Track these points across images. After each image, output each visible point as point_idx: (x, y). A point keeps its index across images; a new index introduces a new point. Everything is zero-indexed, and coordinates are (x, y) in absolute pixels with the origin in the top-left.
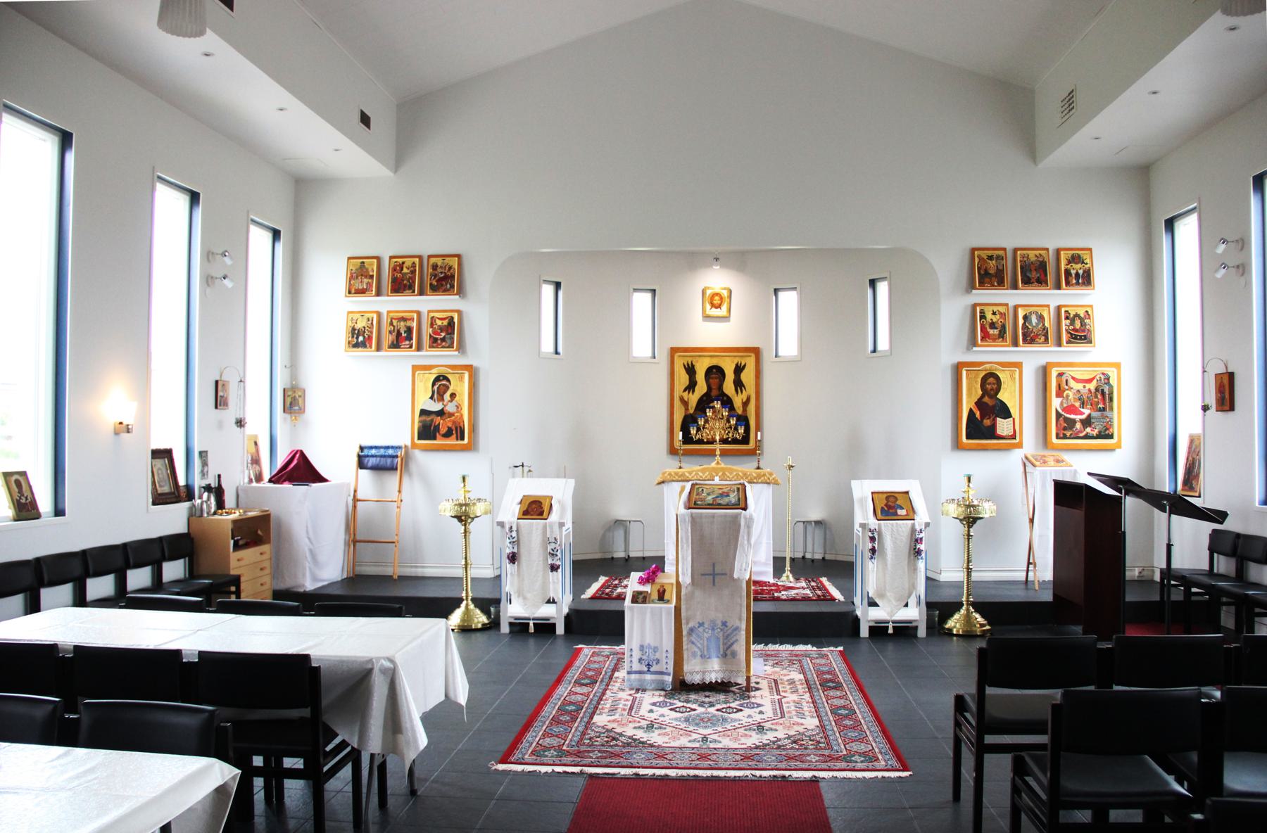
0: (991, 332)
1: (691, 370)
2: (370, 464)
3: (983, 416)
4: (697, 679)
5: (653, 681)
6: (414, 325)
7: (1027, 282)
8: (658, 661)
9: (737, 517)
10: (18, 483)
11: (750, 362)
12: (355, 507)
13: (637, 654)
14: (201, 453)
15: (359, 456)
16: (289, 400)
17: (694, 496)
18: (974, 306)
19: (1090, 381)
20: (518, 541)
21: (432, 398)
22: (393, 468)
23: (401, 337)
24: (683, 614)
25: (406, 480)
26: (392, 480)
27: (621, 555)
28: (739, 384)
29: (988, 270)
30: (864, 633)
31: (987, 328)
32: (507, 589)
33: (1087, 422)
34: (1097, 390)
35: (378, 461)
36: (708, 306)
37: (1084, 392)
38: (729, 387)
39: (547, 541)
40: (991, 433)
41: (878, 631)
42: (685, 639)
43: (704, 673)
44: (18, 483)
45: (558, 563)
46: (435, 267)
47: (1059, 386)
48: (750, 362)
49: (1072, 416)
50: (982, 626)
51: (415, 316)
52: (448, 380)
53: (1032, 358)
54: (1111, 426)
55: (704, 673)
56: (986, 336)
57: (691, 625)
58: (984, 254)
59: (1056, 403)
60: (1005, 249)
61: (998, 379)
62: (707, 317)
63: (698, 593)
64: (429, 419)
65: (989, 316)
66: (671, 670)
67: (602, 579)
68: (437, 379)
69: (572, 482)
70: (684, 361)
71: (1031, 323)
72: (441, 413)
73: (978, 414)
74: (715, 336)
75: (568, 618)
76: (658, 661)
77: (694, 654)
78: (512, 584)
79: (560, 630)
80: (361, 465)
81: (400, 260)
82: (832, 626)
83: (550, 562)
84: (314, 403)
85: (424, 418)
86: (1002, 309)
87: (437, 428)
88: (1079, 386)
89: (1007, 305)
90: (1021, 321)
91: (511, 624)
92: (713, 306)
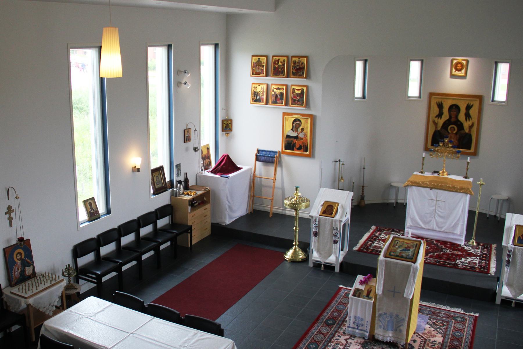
1: (440, 106)
2: (262, 160)
4: (380, 338)
5: (359, 333)
6: (284, 92)
8: (363, 325)
9: (410, 266)
10: (90, 204)
12: (254, 180)
13: (352, 320)
14: (177, 166)
15: (256, 155)
16: (225, 125)
17: (392, 248)
20: (319, 226)
21: (292, 129)
22: (273, 162)
23: (278, 99)
24: (377, 307)
25: (279, 169)
26: (272, 168)
28: (468, 116)
30: (498, 301)
32: (312, 248)
35: (265, 157)
36: (454, 70)
38: (462, 117)
39: (332, 229)
41: (506, 302)
42: (376, 318)
43: (384, 336)
44: (90, 204)
46: (295, 63)
48: (476, 104)
51: (285, 87)
52: (300, 121)
55: (384, 336)
57: (381, 312)
62: (452, 76)
64: (291, 140)
66: (368, 330)
67: (373, 227)
68: (295, 121)
69: (352, 194)
70: (436, 101)
72: (296, 138)
75: (342, 264)
77: (380, 326)
78: (314, 246)
79: (337, 270)
80: (258, 159)
81: (277, 58)
84: (236, 126)
85: (288, 139)
87: (294, 145)
91: (314, 263)
92: (457, 70)
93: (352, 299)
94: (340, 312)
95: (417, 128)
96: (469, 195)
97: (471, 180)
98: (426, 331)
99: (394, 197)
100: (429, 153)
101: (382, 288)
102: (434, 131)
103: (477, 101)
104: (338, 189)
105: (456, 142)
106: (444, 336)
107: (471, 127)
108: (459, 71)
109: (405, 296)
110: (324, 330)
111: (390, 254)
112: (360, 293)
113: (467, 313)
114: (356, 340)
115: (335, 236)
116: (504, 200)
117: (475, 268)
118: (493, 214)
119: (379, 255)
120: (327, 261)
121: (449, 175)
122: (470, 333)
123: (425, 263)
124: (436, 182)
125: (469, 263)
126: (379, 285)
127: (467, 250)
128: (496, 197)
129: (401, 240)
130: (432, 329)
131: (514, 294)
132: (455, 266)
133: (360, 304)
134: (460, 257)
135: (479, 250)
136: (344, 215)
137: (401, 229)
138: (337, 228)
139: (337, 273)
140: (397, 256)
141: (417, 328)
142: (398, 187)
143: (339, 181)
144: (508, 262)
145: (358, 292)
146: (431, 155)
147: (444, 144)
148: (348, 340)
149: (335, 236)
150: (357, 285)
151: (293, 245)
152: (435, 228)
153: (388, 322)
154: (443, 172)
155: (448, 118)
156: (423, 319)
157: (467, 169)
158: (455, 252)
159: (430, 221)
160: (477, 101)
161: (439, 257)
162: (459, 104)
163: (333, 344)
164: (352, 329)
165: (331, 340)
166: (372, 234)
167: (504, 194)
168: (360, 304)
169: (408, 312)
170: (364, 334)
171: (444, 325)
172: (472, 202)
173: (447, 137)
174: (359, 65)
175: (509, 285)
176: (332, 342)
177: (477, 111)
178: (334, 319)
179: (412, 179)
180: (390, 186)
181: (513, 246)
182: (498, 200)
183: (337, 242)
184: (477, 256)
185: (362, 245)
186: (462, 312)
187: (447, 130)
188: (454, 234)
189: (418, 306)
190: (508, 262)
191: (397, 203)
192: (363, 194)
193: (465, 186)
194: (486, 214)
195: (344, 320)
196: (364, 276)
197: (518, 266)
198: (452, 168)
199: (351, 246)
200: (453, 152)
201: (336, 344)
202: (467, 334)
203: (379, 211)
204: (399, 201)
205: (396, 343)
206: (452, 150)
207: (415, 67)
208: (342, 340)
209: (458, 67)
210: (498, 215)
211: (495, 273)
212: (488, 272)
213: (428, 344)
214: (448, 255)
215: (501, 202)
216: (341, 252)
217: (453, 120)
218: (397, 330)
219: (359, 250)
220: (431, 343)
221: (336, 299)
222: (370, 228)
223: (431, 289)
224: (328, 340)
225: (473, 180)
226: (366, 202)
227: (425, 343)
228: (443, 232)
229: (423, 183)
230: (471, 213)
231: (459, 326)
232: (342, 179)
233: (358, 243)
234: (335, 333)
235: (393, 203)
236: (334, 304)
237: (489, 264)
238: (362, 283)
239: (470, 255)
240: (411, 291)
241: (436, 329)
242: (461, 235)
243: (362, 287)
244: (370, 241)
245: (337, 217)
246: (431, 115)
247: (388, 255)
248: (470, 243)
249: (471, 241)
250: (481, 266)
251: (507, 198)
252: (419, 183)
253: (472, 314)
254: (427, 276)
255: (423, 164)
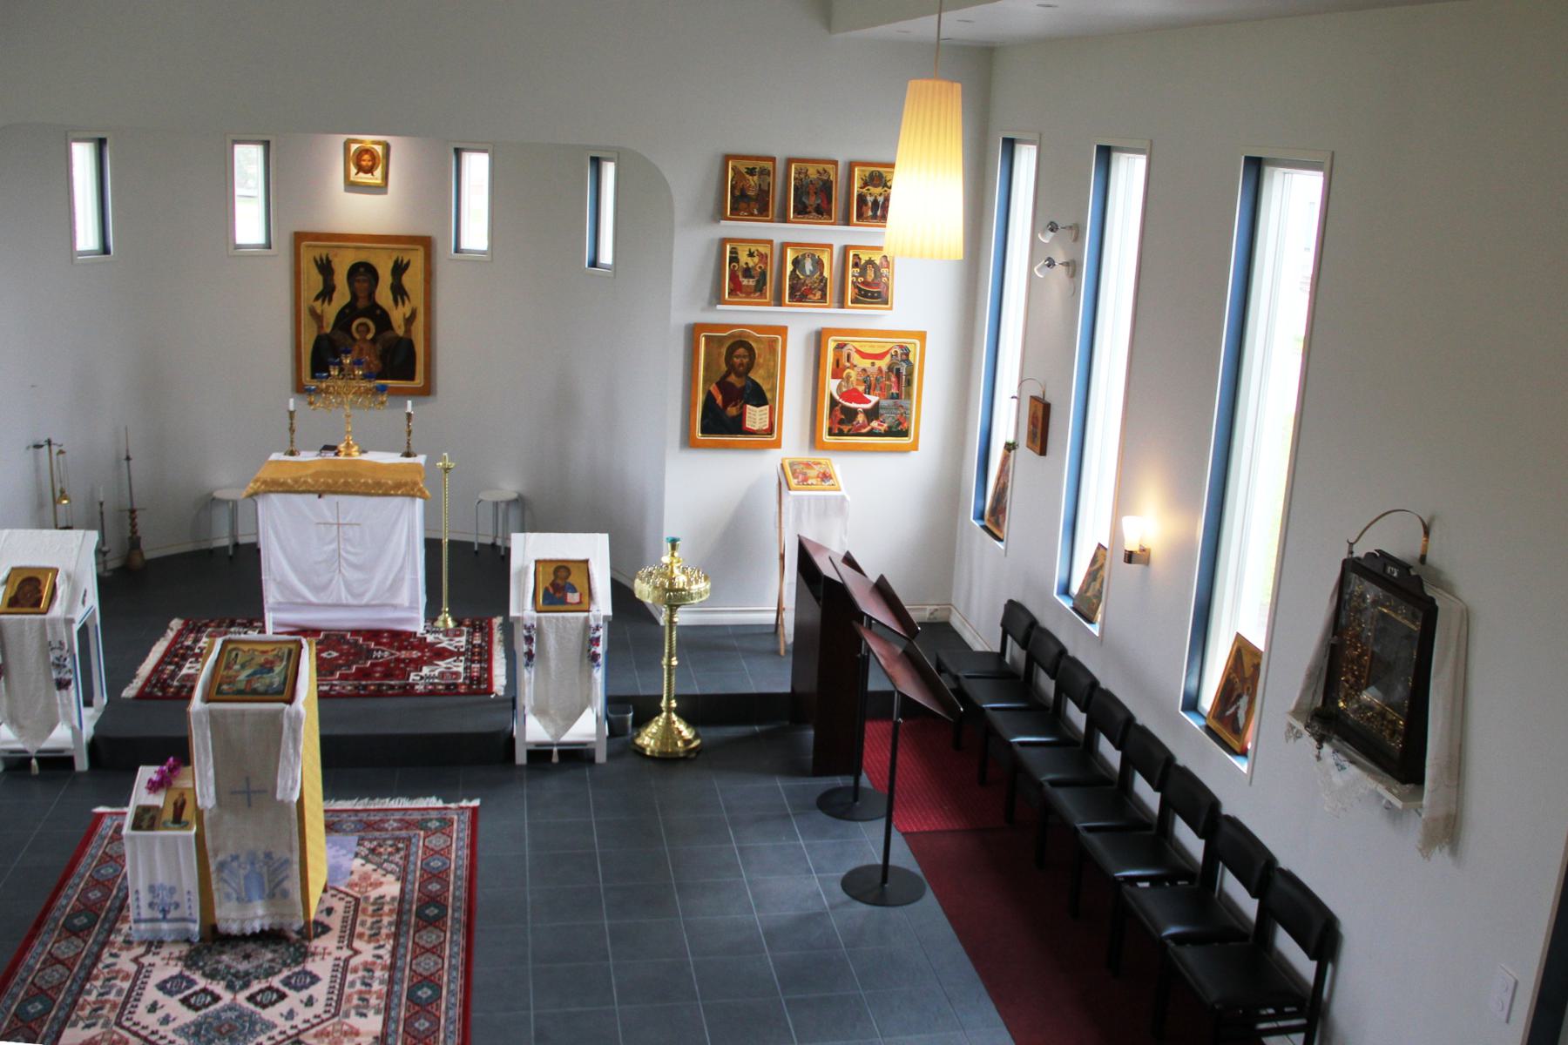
0: (745, 282)
1: (325, 268)
3: (726, 403)
4: (234, 928)
5: (171, 931)
7: (802, 211)
8: (177, 906)
9: (276, 717)
11: (417, 259)
13: (145, 898)
17: (222, 672)
18: (724, 241)
19: (880, 356)
24: (209, 844)
27: (225, 542)
28: (399, 292)
29: (747, 191)
30: (521, 758)
31: (742, 277)
33: (873, 414)
34: (890, 369)
36: (353, 170)
37: (873, 371)
38: (384, 296)
39: (47, 647)
40: (736, 426)
41: (539, 755)
42: (213, 877)
45: (69, 676)
47: (837, 362)
48: (417, 259)
49: (853, 405)
50: (687, 742)
53: (798, 323)
54: (907, 419)
55: (243, 921)
56: (736, 288)
57: (221, 857)
58: (743, 166)
59: (832, 386)
60: (773, 159)
61: (750, 349)
62: (351, 186)
63: (227, 817)
65: (743, 257)
66: (197, 916)
67: (176, 624)
69: (94, 536)
70: (313, 251)
71: (803, 271)
73: (719, 399)
74: (363, 213)
75: (93, 746)
76: (177, 906)
77: (228, 896)
79: (82, 764)
82: (470, 752)
83: (55, 675)
86: (763, 249)
88: (866, 363)
89: (770, 242)
90: (789, 268)
92: (360, 169)
93: (132, 838)
94: (105, 885)
95: (269, 329)
96: (419, 502)
97: (421, 459)
98: (355, 878)
99: (226, 531)
100: (306, 398)
101: (212, 789)
102: (315, 335)
103: (419, 250)
104: (56, 527)
105: (376, 364)
106: (403, 878)
107: (409, 321)
108: (366, 172)
109: (279, 796)
110: (65, 950)
111: (219, 692)
112: (153, 819)
113: (452, 805)
114: (165, 952)
115: (59, 666)
116: (509, 503)
117: (456, 686)
118: (489, 541)
119: (189, 697)
120: (46, 745)
121: (364, 452)
122: (466, 852)
123: (322, 696)
124: (331, 474)
125: (442, 675)
126: (202, 782)
127: (432, 645)
128: (489, 496)
129: (246, 648)
130: (370, 867)
131: (552, 731)
132: (408, 690)
133: (157, 847)
134: (418, 664)
135: (464, 639)
136: (77, 600)
137: (254, 617)
138: (61, 643)
139: (81, 774)
140: (240, 692)
141: (330, 875)
142: (235, 503)
143: (56, 502)
144: (530, 655)
145: (147, 817)
146: (311, 403)
147: (341, 370)
148: (350, 953)
149: (59, 666)
150: (141, 796)
151: (659, 712)
152: (345, 598)
153: (246, 877)
154: (348, 446)
155: (347, 299)
156: (342, 847)
157: (409, 433)
158: (403, 654)
159: (331, 581)
160: (419, 250)
161: (364, 674)
162: (373, 260)
163: (98, 983)
164: (149, 926)
165: (90, 973)
166: (174, 641)
167: (509, 488)
168: (157, 847)
169: (296, 838)
170: (187, 930)
171: (398, 850)
172: (430, 516)
173: (347, 352)
174: (82, 156)
175: (540, 712)
176: (96, 978)
177: (421, 277)
178: (90, 910)
179: (266, 473)
180: (210, 502)
181: (536, 615)
182: (496, 504)
183: (69, 682)
184: (459, 654)
185: (148, 680)
186: (440, 804)
187: (348, 330)
188: (395, 607)
189: (322, 815)
190: (530, 655)
191: (236, 545)
192: (134, 532)
193: (407, 478)
194: (472, 544)
195: (122, 905)
196: (157, 768)
197: (553, 664)
198: (371, 434)
199: (114, 688)
200: (367, 391)
201: (109, 980)
202: (458, 856)
203: (178, 576)
204: (243, 540)
205: (281, 930)
206: (365, 384)
207: (248, 161)
208: (125, 963)
209: (364, 161)
210: (499, 542)
211: (507, 688)
212: (489, 691)
213: (364, 911)
214: (386, 664)
215: (502, 507)
216: (88, 713)
217: (362, 304)
218: (275, 893)
219: (142, 695)
220: (374, 903)
221: (91, 850)
222: (166, 627)
223: (346, 763)
224: (82, 974)
225: (427, 461)
226: (148, 555)
227: (356, 911)
228: (367, 606)
229: (296, 481)
230: (432, 546)
231: (437, 842)
232: (63, 495)
233: (134, 676)
234: (101, 949)
235: (225, 548)
236: (86, 867)
237: (489, 670)
238: (153, 787)
239: (442, 654)
240: (295, 781)
241: (380, 866)
242: (413, 607)
243: (157, 800)
244: (170, 663)
245: (58, 610)
246: (304, 294)
247: (214, 695)
248: (439, 624)
249: (441, 618)
250: (471, 678)
251: (514, 496)
252: (284, 484)
253: (464, 803)
254: (327, 732)
255: (292, 430)
